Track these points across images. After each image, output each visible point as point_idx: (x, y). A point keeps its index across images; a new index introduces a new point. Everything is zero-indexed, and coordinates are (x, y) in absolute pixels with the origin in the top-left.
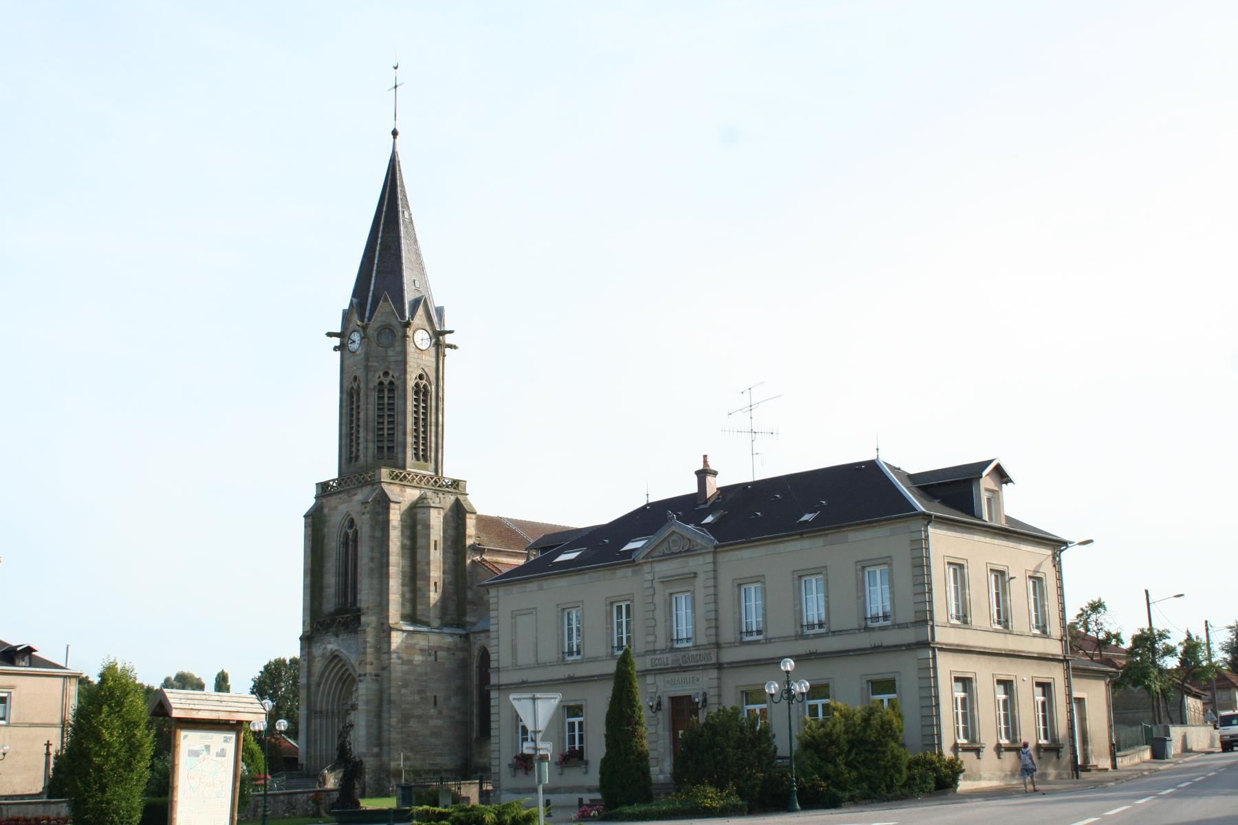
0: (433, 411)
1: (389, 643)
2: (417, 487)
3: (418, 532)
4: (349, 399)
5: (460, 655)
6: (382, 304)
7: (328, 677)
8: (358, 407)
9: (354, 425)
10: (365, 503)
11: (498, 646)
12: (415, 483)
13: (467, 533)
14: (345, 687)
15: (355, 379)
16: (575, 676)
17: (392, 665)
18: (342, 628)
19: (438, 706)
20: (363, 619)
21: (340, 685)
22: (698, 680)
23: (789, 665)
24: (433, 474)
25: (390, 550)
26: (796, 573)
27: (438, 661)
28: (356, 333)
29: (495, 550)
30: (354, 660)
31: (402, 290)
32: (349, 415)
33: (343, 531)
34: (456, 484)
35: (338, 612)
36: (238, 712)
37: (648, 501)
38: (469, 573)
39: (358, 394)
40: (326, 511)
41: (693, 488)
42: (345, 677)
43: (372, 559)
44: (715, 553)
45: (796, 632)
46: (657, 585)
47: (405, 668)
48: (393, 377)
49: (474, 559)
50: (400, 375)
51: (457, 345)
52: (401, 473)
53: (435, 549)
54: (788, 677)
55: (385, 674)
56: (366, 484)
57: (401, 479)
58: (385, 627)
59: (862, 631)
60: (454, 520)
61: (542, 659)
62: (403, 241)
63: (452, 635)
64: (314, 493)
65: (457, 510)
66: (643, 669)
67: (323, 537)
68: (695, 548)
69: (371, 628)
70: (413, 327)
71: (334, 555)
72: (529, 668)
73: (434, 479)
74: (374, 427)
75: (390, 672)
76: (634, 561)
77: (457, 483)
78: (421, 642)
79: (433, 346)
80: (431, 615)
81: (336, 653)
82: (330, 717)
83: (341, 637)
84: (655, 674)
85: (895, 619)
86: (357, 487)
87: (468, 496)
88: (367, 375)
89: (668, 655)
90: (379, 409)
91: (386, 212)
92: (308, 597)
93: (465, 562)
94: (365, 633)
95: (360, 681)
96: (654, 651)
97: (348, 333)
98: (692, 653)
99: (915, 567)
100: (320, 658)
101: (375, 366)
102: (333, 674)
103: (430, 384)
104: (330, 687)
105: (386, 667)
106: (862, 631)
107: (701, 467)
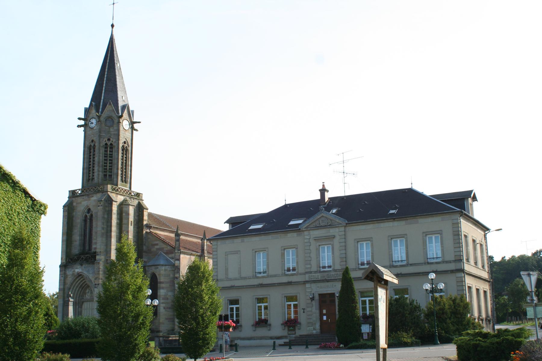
0: (130, 159)
2: (122, 195)
3: (123, 217)
6: (108, 106)
7: (75, 285)
8: (94, 155)
9: (91, 163)
11: (217, 268)
12: (121, 193)
13: (144, 218)
14: (83, 291)
15: (93, 141)
16: (263, 284)
20: (97, 257)
22: (335, 286)
23: (432, 276)
24: (129, 189)
25: (112, 224)
26: (389, 237)
28: (93, 119)
29: (156, 227)
30: (91, 277)
34: (138, 195)
35: (80, 254)
36: (387, 275)
37: (285, 203)
38: (145, 237)
39: (94, 148)
40: (74, 204)
41: (318, 197)
42: (83, 285)
43: (103, 228)
44: (345, 226)
45: (390, 264)
46: (312, 241)
48: (112, 141)
49: (147, 231)
50: (116, 141)
51: (138, 130)
52: (116, 188)
53: (131, 225)
54: (432, 282)
56: (99, 192)
57: (116, 190)
59: (426, 264)
60: (137, 212)
61: (243, 275)
62: (117, 77)
65: (139, 207)
66: (305, 280)
67: (73, 217)
68: (334, 224)
69: (102, 262)
70: (123, 118)
71: (79, 226)
72: (236, 279)
74: (103, 165)
76: (300, 229)
81: (81, 273)
83: (84, 266)
84: (311, 283)
85: (268, 273)
87: (143, 201)
88: (100, 139)
89: (318, 274)
91: (109, 62)
92: (65, 246)
95: (95, 287)
96: (311, 272)
97: (89, 119)
98: (332, 273)
99: (454, 235)
100: (70, 276)
101: (104, 136)
102: (77, 284)
103: (129, 147)
104: (76, 290)
106: (426, 264)
107: (321, 188)
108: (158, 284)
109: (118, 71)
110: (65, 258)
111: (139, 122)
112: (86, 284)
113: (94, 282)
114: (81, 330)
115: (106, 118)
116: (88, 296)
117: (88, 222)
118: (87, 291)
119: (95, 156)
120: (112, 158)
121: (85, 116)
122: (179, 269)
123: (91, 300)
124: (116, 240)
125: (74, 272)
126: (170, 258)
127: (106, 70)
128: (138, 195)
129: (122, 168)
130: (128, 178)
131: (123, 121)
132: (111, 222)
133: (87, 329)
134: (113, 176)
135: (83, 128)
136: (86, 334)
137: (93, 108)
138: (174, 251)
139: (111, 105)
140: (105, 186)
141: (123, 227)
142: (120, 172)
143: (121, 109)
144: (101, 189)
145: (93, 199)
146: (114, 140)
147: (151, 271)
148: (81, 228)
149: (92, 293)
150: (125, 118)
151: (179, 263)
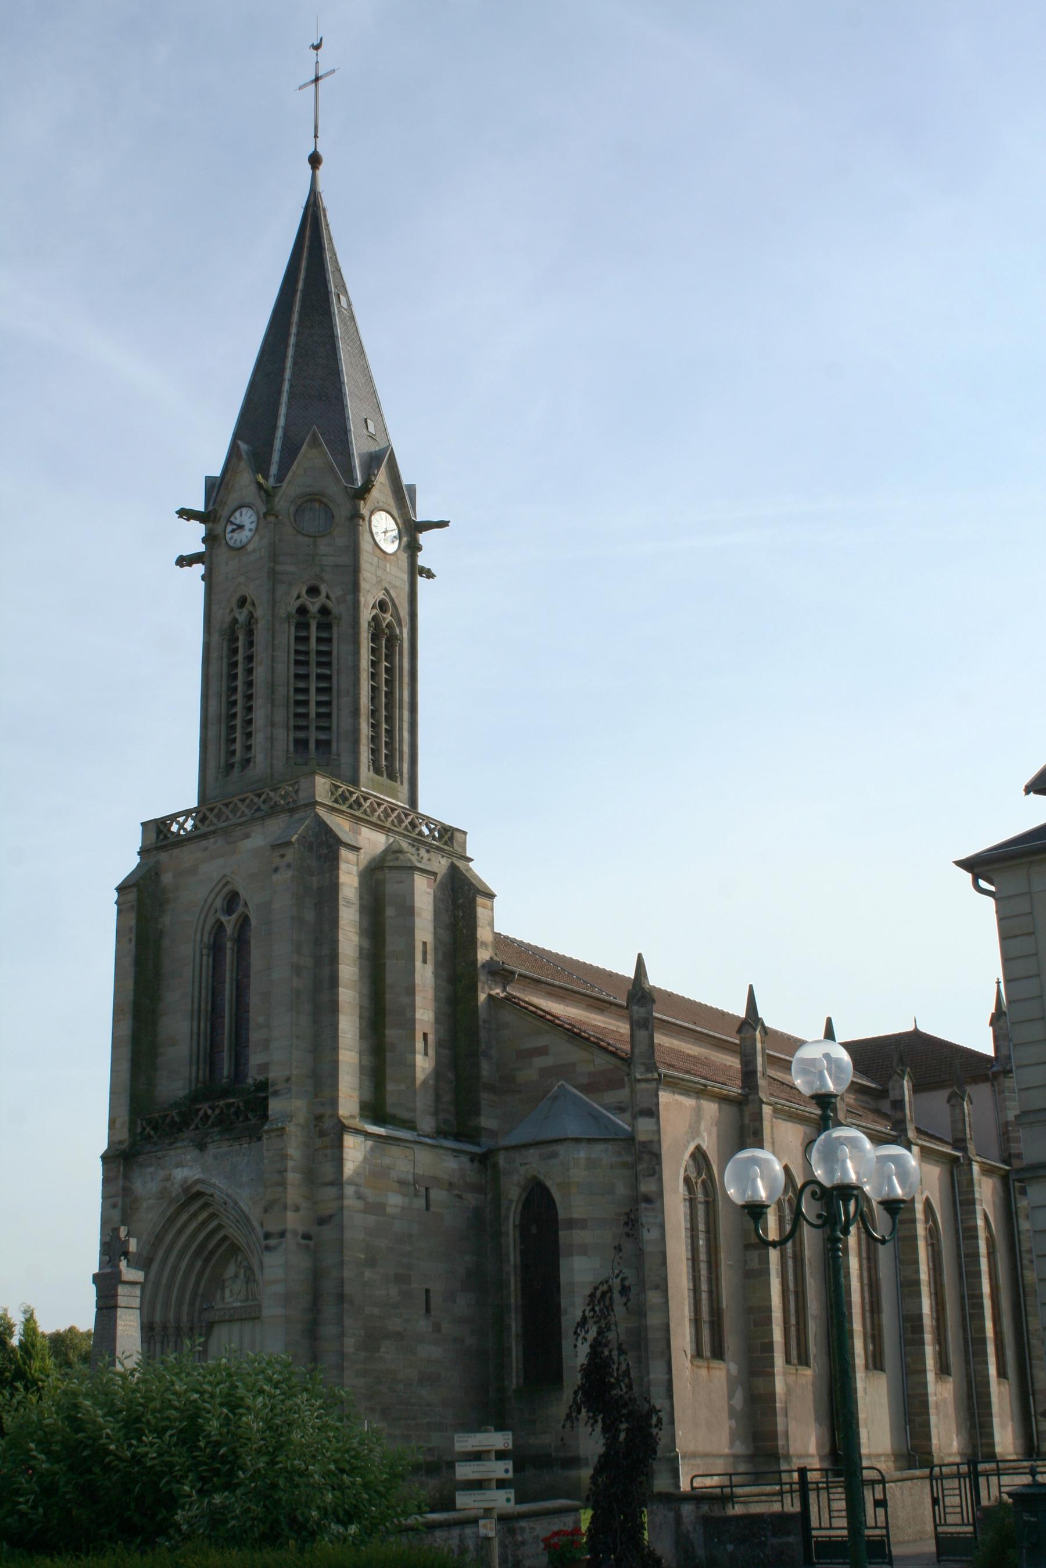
0: (406, 680)
1: (339, 1161)
5: (471, 1199)
8: (250, 658)
9: (239, 696)
10: (281, 845)
13: (478, 936)
17: (345, 1213)
19: (433, 1313)
20: (275, 1106)
21: (199, 1264)
25: (340, 950)
27: (432, 1209)
28: (244, 510)
30: (246, 1199)
31: (345, 431)
33: (211, 921)
35: (195, 1098)
38: (485, 1022)
39: (250, 633)
40: (167, 878)
43: (297, 970)
47: (371, 1220)
48: (328, 597)
49: (493, 992)
51: (433, 571)
52: (351, 793)
53: (425, 961)
55: (327, 1232)
56: (274, 811)
58: (328, 1124)
62: (341, 344)
63: (456, 1153)
65: (453, 890)
73: (410, 818)
75: (341, 1228)
77: (449, 834)
79: (404, 551)
80: (419, 1105)
81: (199, 1187)
82: (172, 1339)
83: (212, 1150)
86: (254, 819)
87: (471, 864)
88: (274, 589)
90: (297, 663)
91: (304, 291)
92: (126, 1065)
94: (281, 1136)
95: (268, 1248)
97: (225, 513)
100: (152, 1201)
103: (400, 625)
104: (175, 1268)
105: (331, 1217)
108: (562, 1233)
109: (345, 324)
110: (127, 1118)
111: (442, 524)
112: (225, 1238)
113: (262, 1225)
114: (171, 1466)
115: (299, 502)
116: (232, 1297)
117: (228, 952)
118: (230, 1271)
119: (254, 664)
121: (211, 503)
122: (657, 1157)
123: (250, 1315)
124: (358, 1025)
126: (607, 1109)
127: (295, 318)
128: (446, 838)
129: (374, 713)
130: (401, 760)
131: (372, 513)
132: (335, 942)
133: (223, 1460)
134: (334, 745)
135: (199, 569)
136: (217, 1499)
137: (243, 464)
138: (628, 1075)
139: (320, 445)
140: (304, 783)
141: (387, 965)
142: (365, 730)
143: (361, 465)
144: (283, 797)
145: (248, 844)
146: (337, 592)
147: (522, 1170)
148: (197, 979)
149: (250, 1278)
150: (381, 504)
151: (655, 1128)
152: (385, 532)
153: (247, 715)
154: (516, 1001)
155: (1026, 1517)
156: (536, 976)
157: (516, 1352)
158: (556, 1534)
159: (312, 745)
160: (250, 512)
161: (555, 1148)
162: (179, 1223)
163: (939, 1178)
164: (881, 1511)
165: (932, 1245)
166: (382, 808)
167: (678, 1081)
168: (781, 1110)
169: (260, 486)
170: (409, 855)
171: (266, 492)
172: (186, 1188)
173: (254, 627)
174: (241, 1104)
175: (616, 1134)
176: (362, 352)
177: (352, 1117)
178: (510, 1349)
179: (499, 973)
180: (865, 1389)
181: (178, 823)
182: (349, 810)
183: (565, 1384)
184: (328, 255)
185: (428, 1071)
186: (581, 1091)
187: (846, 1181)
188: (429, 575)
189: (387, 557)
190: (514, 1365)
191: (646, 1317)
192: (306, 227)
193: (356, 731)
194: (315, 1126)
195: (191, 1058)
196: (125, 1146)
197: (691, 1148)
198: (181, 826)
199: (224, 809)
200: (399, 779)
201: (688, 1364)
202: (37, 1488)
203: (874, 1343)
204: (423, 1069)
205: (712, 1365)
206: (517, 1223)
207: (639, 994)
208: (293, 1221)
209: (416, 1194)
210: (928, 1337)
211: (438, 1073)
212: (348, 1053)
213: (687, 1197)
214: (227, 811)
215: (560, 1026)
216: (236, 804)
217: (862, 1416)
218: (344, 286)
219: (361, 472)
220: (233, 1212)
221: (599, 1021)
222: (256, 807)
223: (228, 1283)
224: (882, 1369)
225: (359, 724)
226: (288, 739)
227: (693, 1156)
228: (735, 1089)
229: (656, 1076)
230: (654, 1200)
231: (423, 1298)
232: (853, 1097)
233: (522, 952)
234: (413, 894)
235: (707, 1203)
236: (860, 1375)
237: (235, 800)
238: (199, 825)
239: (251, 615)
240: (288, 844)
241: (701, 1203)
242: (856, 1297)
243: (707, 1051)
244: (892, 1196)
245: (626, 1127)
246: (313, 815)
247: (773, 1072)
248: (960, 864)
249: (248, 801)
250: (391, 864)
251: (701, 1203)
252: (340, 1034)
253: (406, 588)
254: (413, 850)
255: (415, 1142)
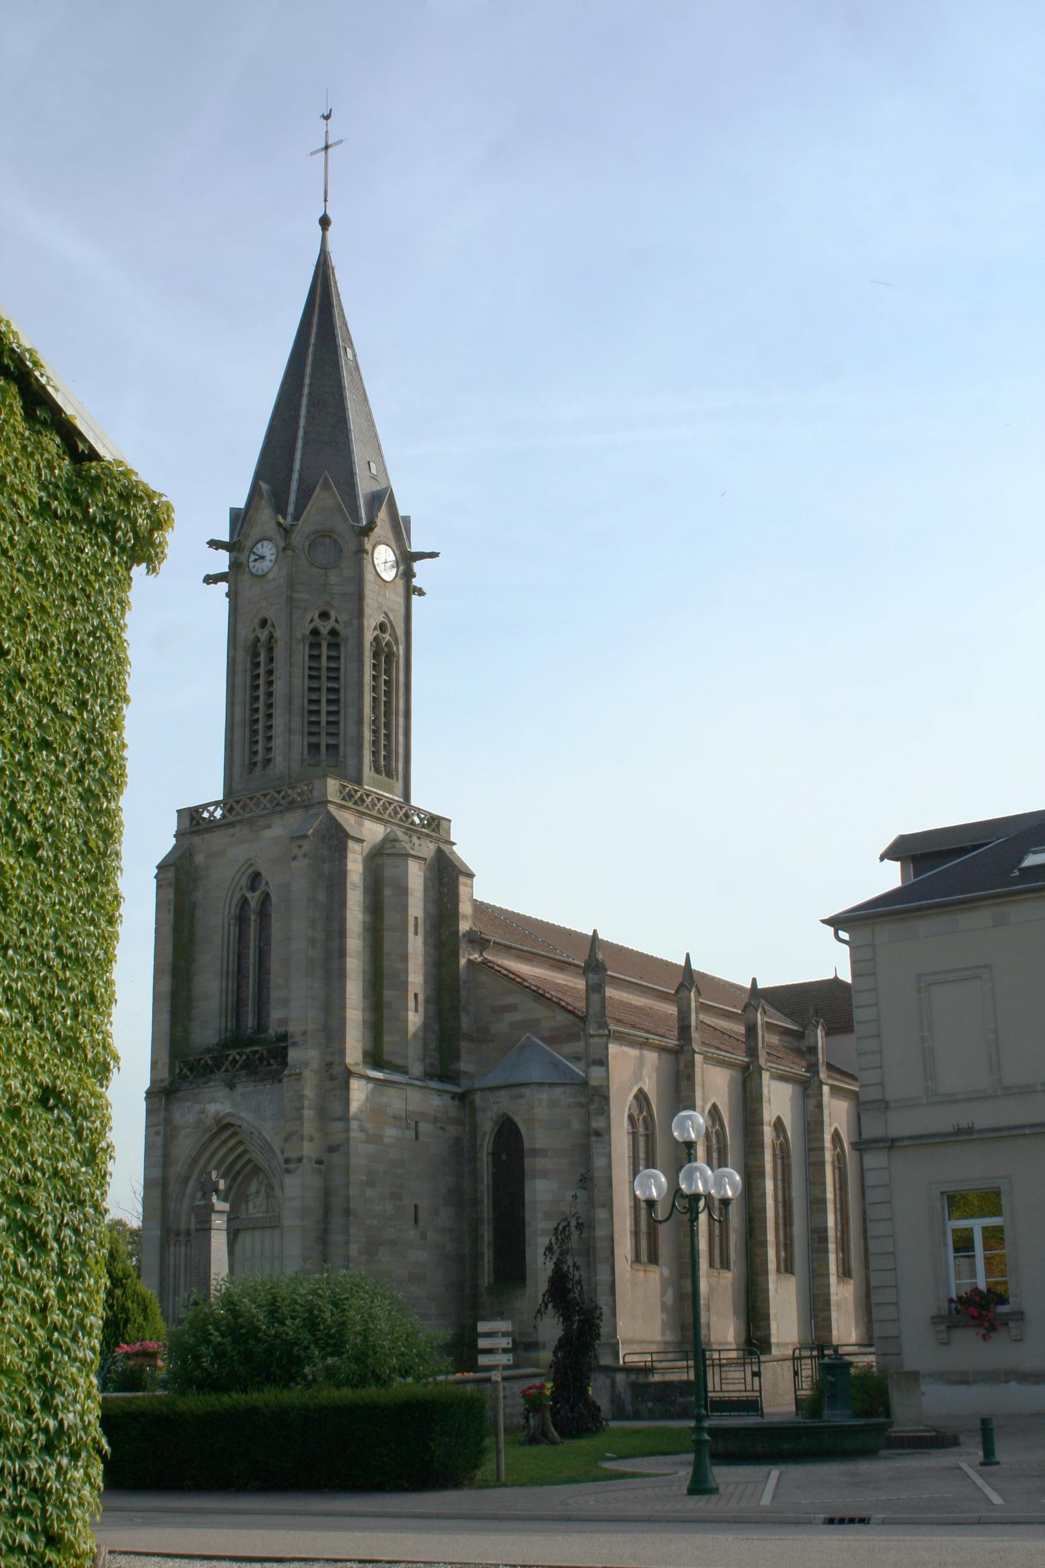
4: (249, 660)
5: (453, 1130)
8: (270, 672)
13: (460, 910)
17: (351, 1143)
18: (244, 1072)
20: (293, 1054)
27: (420, 1139)
28: (265, 543)
30: (270, 1131)
31: (351, 474)
32: (248, 687)
33: (237, 896)
38: (465, 982)
39: (270, 650)
40: (199, 859)
42: (238, 1167)
43: (312, 942)
48: (337, 621)
49: (472, 957)
51: (424, 590)
52: (356, 791)
53: (416, 933)
56: (292, 806)
58: (337, 1070)
63: (440, 1092)
64: (173, 827)
65: (439, 870)
75: (347, 1154)
77: (437, 821)
78: (396, 1101)
79: (401, 578)
83: (240, 1089)
87: (454, 848)
88: (291, 615)
90: (311, 677)
91: (315, 345)
92: (166, 1016)
93: (458, 963)
94: (299, 1080)
95: (288, 1171)
97: (249, 544)
103: (397, 643)
105: (339, 1146)
108: (526, 1160)
111: (433, 555)
112: (250, 1161)
113: (282, 1152)
115: (312, 538)
117: (252, 924)
118: (253, 1188)
119: (273, 678)
120: (339, 683)
122: (606, 1099)
124: (361, 988)
125: (203, 1116)
126: (566, 1058)
127: (308, 369)
130: (397, 760)
131: (374, 547)
132: (343, 919)
134: (341, 748)
135: (223, 587)
138: (584, 1030)
139: (331, 487)
142: (368, 735)
143: (365, 504)
144: (299, 794)
145: (268, 833)
146: (344, 617)
148: (225, 945)
150: (382, 538)
151: (605, 1075)
152: (386, 562)
153: (267, 721)
154: (491, 965)
155: (829, 1378)
156: (508, 943)
157: (487, 1255)
158: (530, 1388)
159: (323, 748)
160: (270, 545)
161: (523, 1090)
162: (212, 1148)
163: (847, 1112)
164: (756, 1379)
165: (840, 1168)
166: (382, 802)
167: (626, 1036)
168: (711, 1058)
169: (279, 525)
170: (404, 843)
171: (286, 530)
172: (218, 1120)
173: (274, 645)
174: (265, 1052)
175: (573, 1079)
176: (366, 399)
177: (357, 1064)
178: (482, 1255)
179: (478, 941)
180: (776, 1290)
181: (208, 811)
182: (354, 807)
183: (527, 1282)
184: (336, 311)
185: (418, 1025)
186: (543, 1042)
187: (697, 1192)
188: (421, 593)
189: (387, 584)
190: (486, 1266)
191: (594, 1229)
192: (317, 285)
193: (360, 737)
194: (326, 1071)
195: (221, 1011)
196: (166, 1083)
197: (635, 1090)
198: (212, 814)
199: (248, 801)
200: (395, 777)
201: (628, 1268)
202: (212, 1354)
203: (786, 1251)
204: (414, 1023)
205: (648, 1269)
206: (490, 1150)
207: (594, 964)
208: (309, 1149)
209: (408, 1127)
210: (832, 1246)
211: (426, 1026)
212: (355, 1012)
213: (631, 1131)
214: (251, 804)
215: (527, 987)
216: (259, 799)
217: (772, 1311)
218: (350, 339)
219: (365, 511)
220: (258, 1141)
221: (560, 979)
222: (275, 802)
223: (251, 1197)
224: (792, 1273)
225: (363, 731)
226: (303, 744)
227: (636, 1097)
228: (672, 1042)
229: (606, 1032)
230: (603, 1135)
231: (413, 1211)
232: (778, 1038)
233: (496, 918)
234: (407, 877)
235: (647, 1135)
236: (772, 1277)
237: (258, 794)
238: (227, 814)
239: (271, 637)
240: (305, 837)
241: (642, 1135)
242: (770, 1213)
243: (651, 1001)
244: (726, 1197)
245: (581, 1073)
246: (325, 811)
247: (708, 1018)
248: (824, 922)
249: (268, 797)
250: (389, 851)
251: (642, 1135)
252: (347, 996)
253: (402, 611)
254: (406, 838)
255: (407, 1084)
